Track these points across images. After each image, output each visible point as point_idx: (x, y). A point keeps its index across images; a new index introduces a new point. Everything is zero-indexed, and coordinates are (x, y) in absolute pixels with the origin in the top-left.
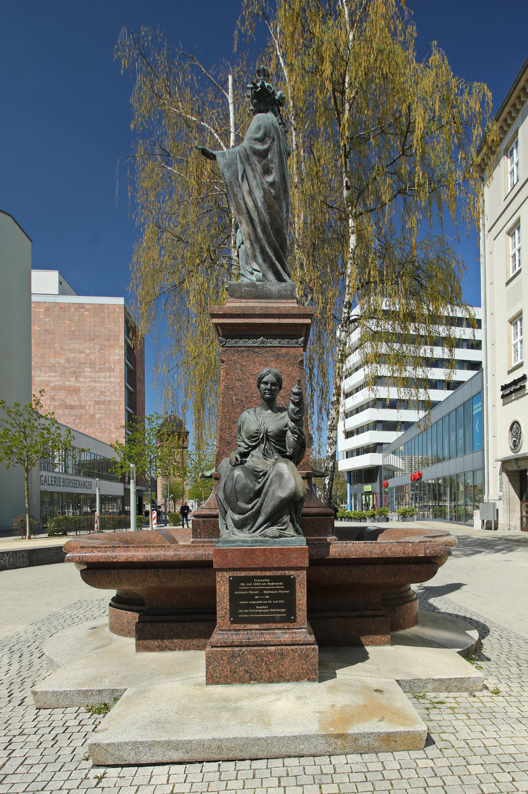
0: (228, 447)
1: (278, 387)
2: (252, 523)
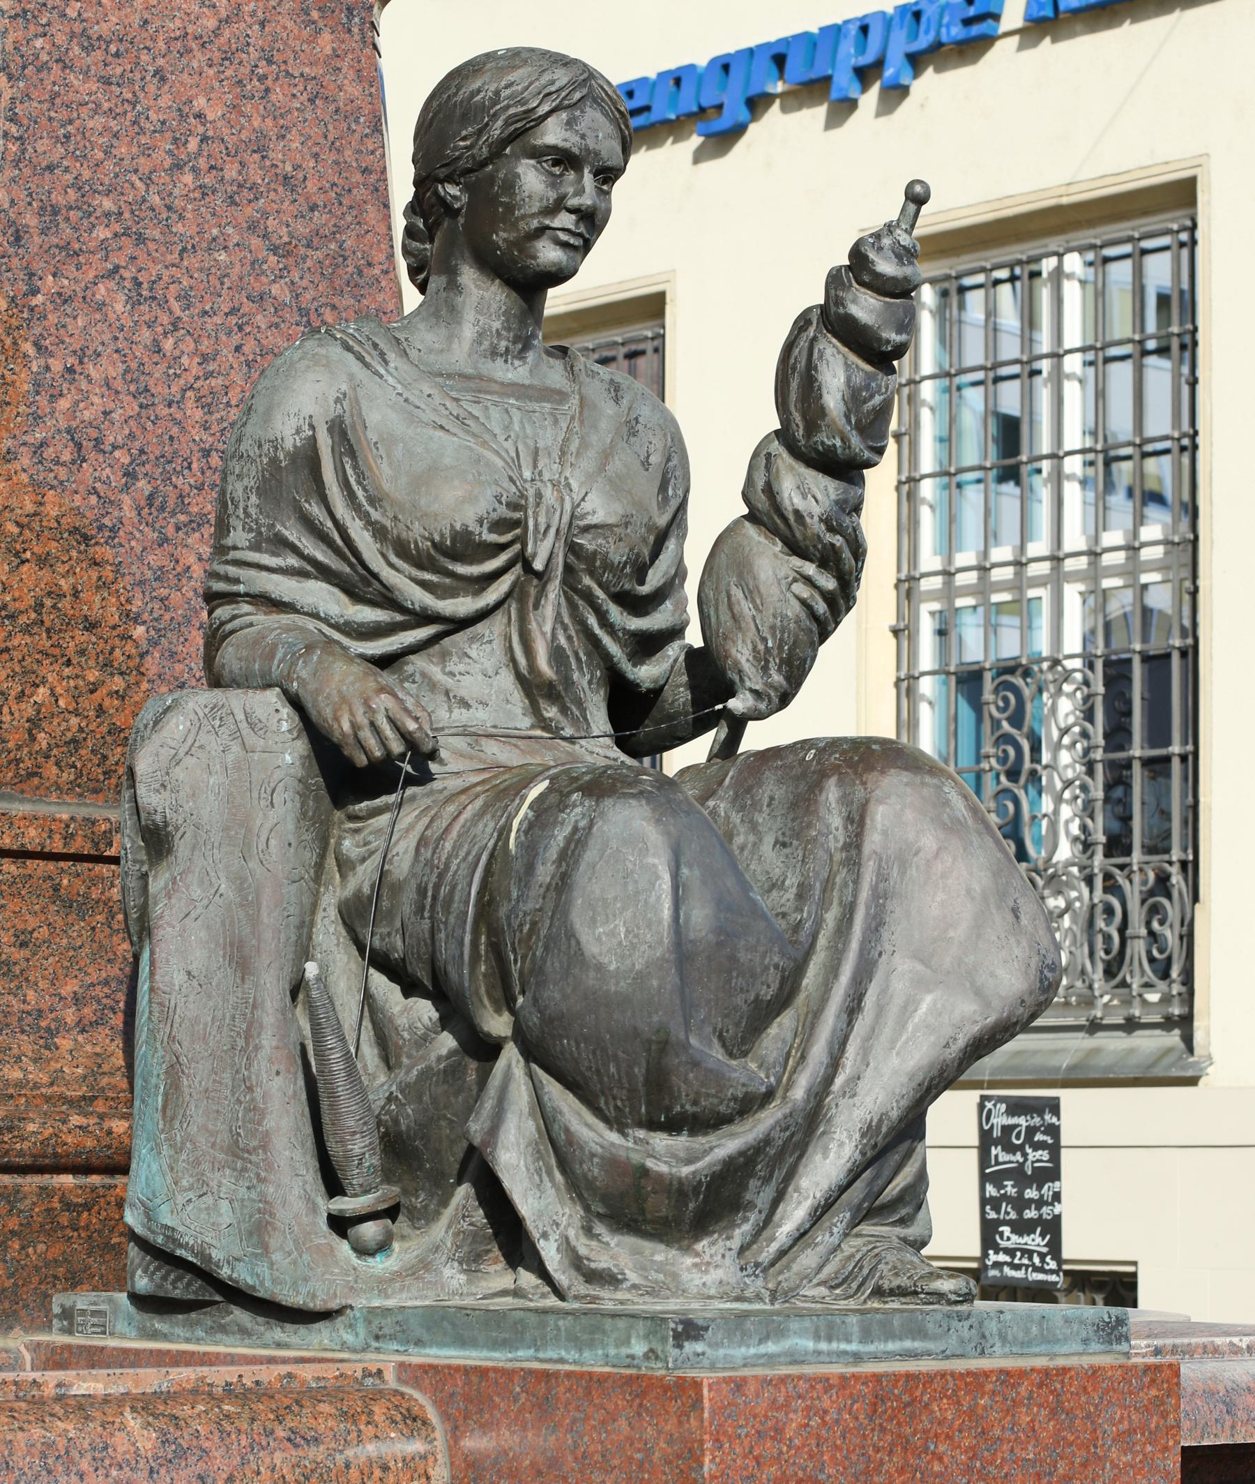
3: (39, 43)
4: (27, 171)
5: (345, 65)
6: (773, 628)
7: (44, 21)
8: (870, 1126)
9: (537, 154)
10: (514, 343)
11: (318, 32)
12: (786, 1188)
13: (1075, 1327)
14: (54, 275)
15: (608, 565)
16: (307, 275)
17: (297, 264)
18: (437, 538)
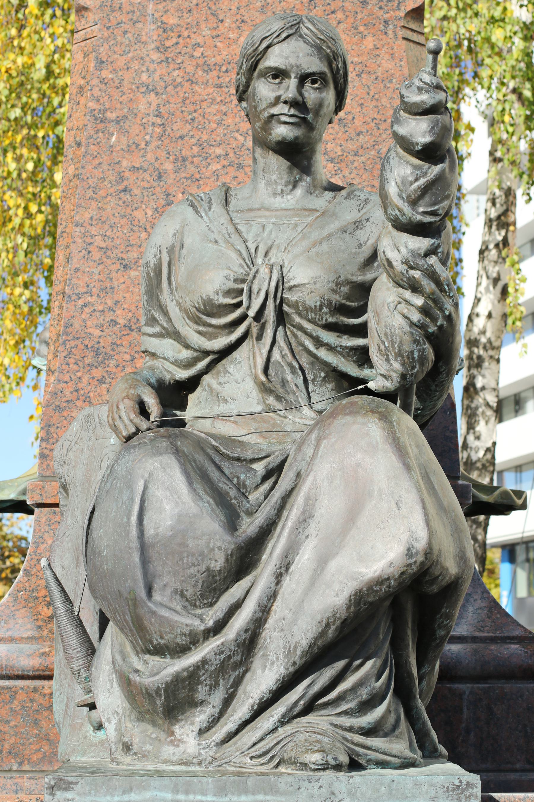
0: (98, 373)
1: (330, 96)
2: (217, 698)
3: (176, 73)
4: (166, 141)
5: (382, 52)
6: (386, 334)
7: (179, 61)
8: (289, 650)
9: (263, 75)
10: (286, 186)
11: (364, 37)
12: (236, 691)
13: (425, 788)
14: (183, 193)
15: (308, 309)
16: (355, 172)
17: (347, 166)
18: (197, 305)
